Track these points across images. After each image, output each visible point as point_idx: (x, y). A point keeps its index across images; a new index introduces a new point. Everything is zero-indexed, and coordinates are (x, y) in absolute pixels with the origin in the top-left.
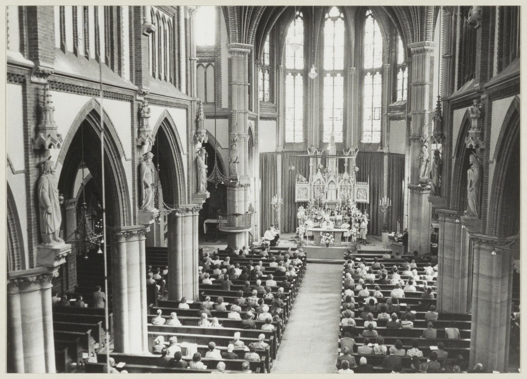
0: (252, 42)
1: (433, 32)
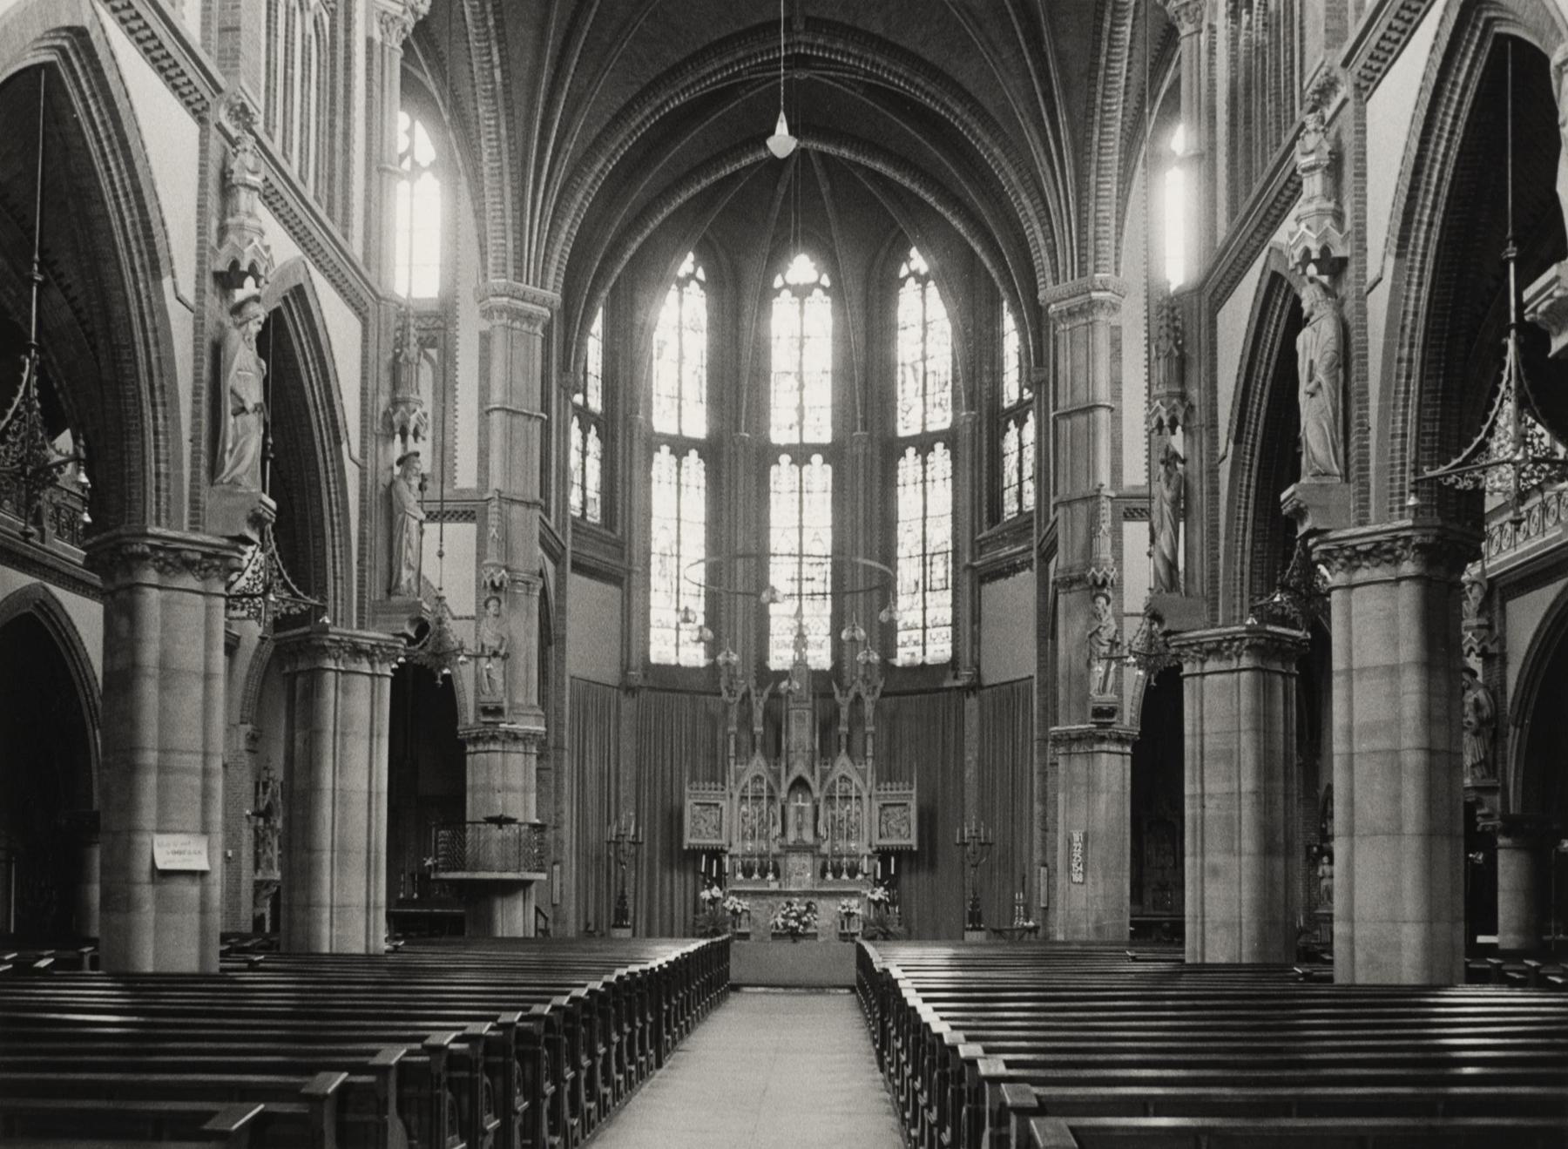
0: (555, 287)
1: (1117, 248)
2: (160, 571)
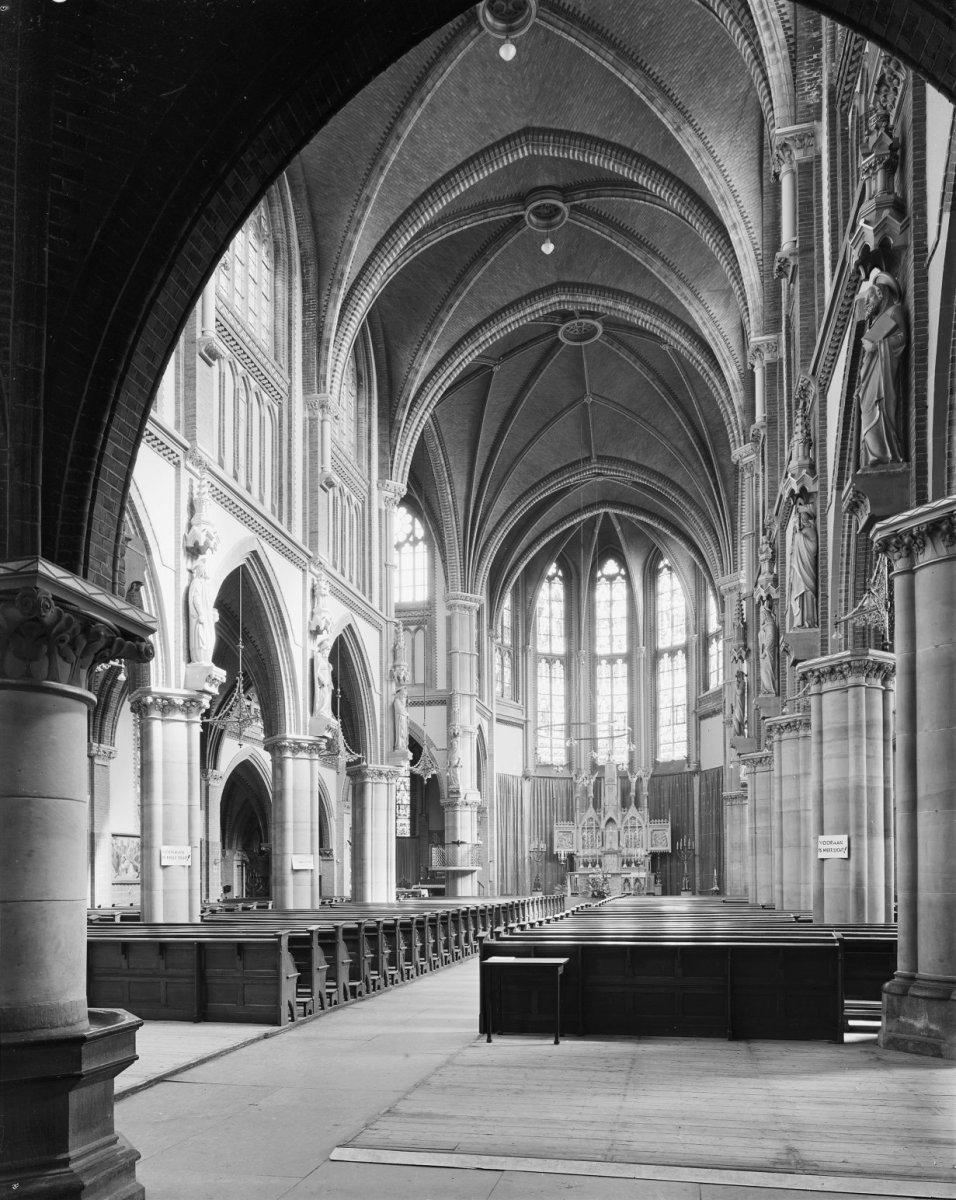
2: (293, 752)
